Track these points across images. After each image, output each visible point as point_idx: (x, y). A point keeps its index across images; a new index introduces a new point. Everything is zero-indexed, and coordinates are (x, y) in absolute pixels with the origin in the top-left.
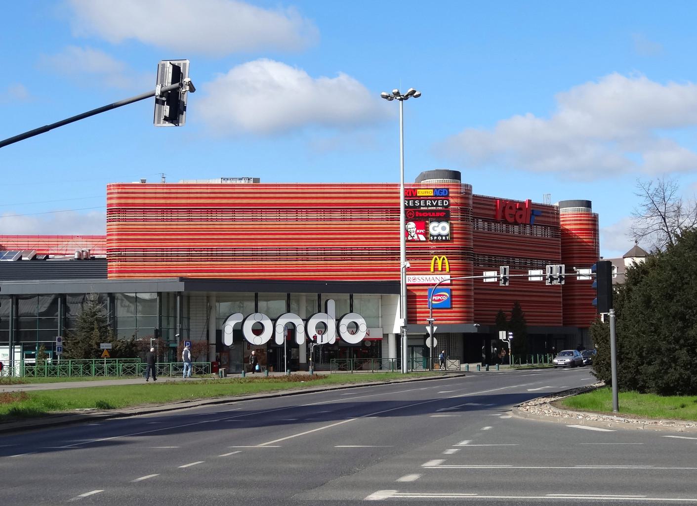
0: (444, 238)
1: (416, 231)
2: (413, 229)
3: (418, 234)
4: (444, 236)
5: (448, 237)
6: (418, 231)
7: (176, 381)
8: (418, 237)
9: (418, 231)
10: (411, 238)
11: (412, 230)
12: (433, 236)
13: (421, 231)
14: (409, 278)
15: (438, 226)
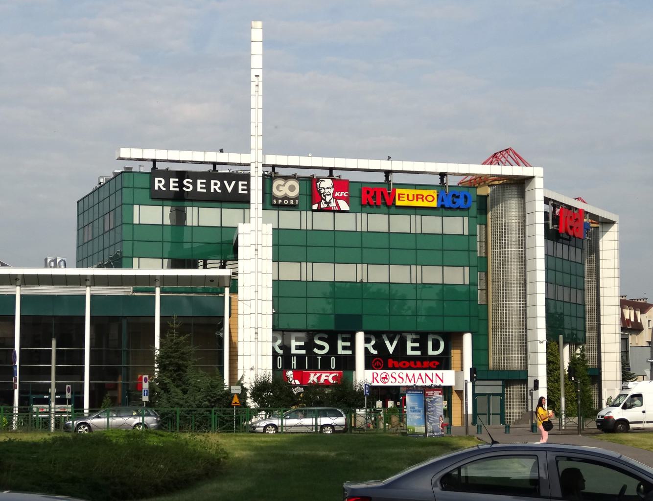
0: (292, 202)
1: (334, 193)
2: (329, 190)
3: (336, 198)
4: (292, 199)
5: (297, 201)
6: (337, 194)
7: (16, 390)
8: (337, 204)
9: (337, 194)
10: (326, 206)
11: (327, 191)
12: (277, 199)
13: (342, 193)
14: (375, 375)
15: (284, 185)
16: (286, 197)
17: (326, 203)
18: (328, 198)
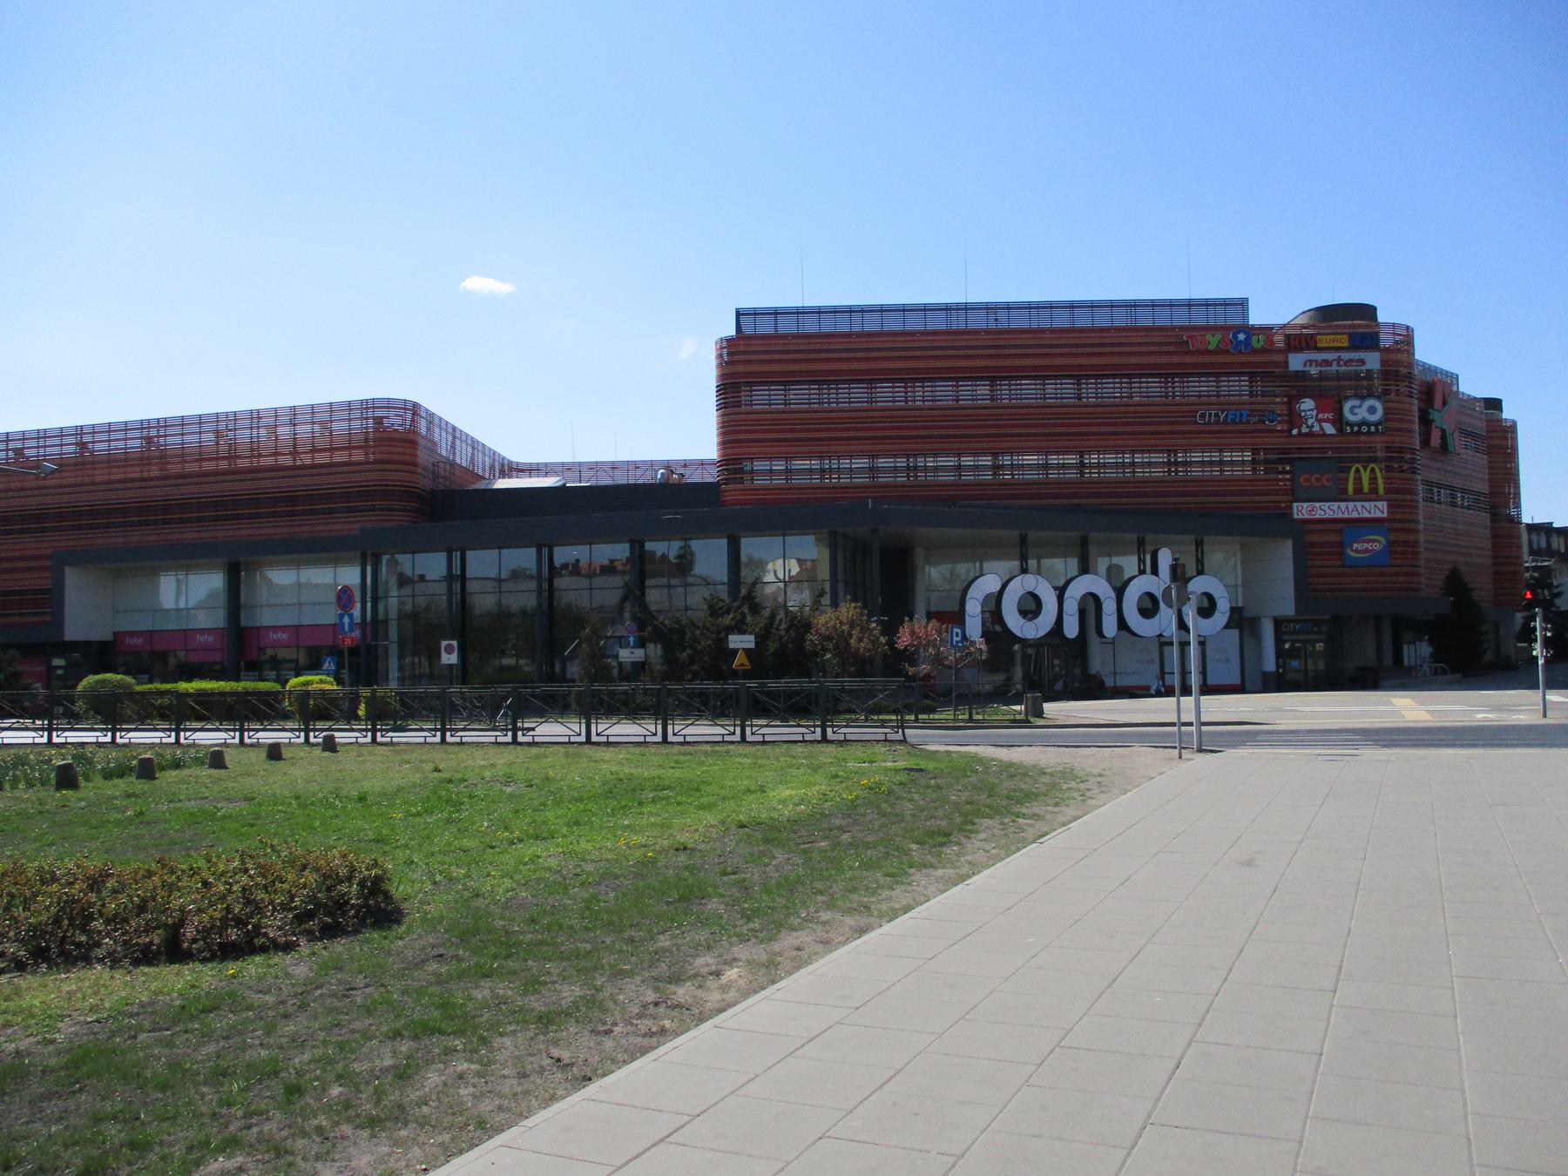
1: (1317, 416)
3: (1320, 421)
6: (1320, 416)
8: (1322, 428)
9: (1320, 416)
11: (1308, 413)
12: (1351, 425)
13: (1326, 415)
15: (1360, 406)
16: (1364, 423)
17: (1308, 427)
18: (1310, 422)
